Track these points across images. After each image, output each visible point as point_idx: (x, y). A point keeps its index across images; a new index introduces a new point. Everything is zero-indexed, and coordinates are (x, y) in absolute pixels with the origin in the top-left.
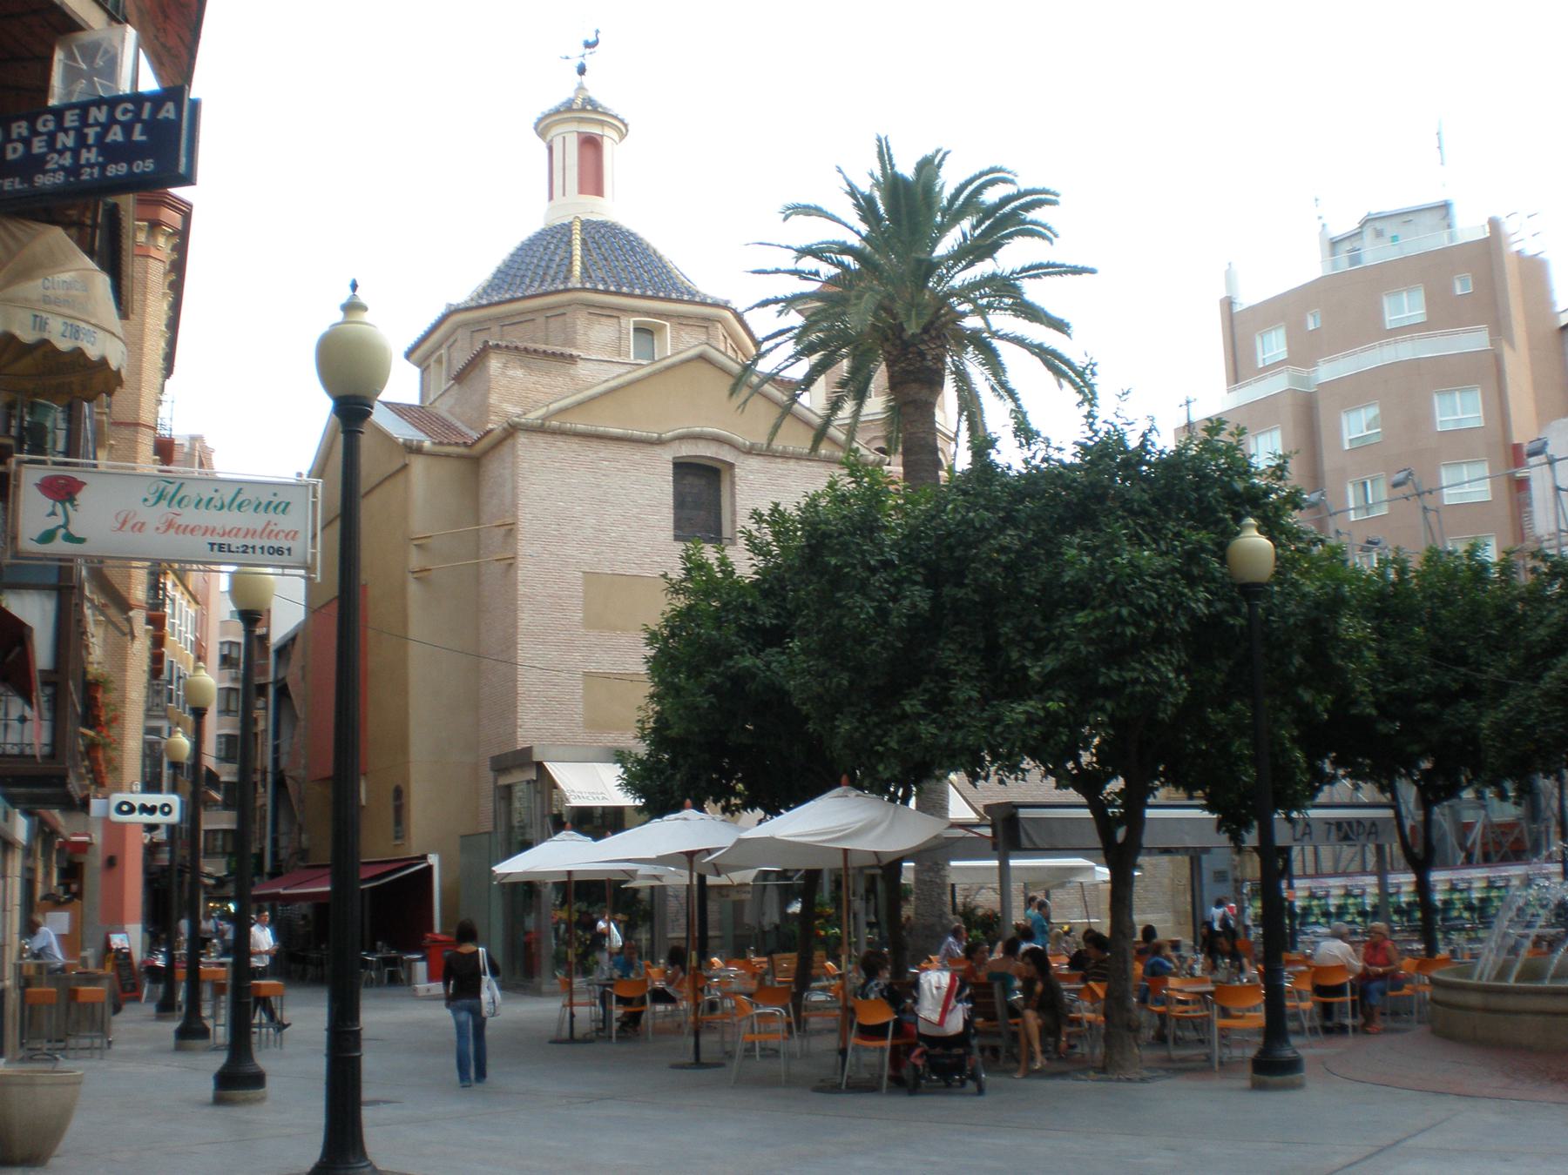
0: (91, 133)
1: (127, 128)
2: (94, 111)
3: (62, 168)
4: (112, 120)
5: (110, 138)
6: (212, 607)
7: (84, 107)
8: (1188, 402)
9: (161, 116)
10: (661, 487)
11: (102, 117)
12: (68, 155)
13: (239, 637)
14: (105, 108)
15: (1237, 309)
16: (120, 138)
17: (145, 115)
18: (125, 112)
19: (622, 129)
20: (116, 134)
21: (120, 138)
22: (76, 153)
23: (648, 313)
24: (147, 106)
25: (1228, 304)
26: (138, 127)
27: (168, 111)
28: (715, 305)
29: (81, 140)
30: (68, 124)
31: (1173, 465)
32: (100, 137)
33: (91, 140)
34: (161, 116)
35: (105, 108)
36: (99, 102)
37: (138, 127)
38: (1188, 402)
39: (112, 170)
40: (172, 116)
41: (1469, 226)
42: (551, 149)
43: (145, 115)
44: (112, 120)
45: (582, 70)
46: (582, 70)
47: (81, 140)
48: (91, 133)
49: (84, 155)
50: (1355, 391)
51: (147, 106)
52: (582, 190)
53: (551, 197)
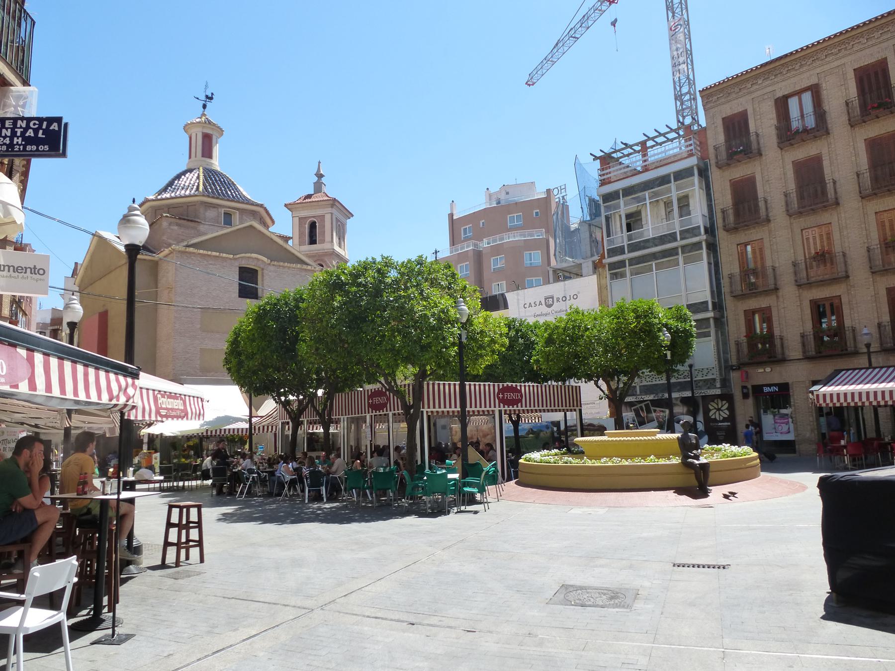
0: (19, 131)
1: (36, 131)
2: (19, 122)
3: (5, 144)
4: (28, 127)
5: (27, 134)
6: (33, 318)
7: (15, 120)
8: (436, 252)
9: (51, 128)
10: (233, 279)
11: (24, 125)
12: (8, 139)
13: (809, 326)
14: (25, 122)
15: (455, 218)
16: (32, 135)
17: (44, 127)
18: (34, 124)
19: (221, 131)
20: (30, 133)
21: (32, 135)
22: (12, 140)
23: (230, 208)
24: (45, 124)
25: (451, 216)
26: (41, 132)
27: (55, 126)
28: (258, 205)
29: (14, 134)
30: (7, 126)
31: (238, 384)
32: (23, 134)
33: (19, 134)
34: (51, 128)
35: (25, 122)
36: (22, 119)
37: (41, 132)
38: (436, 252)
39: (29, 148)
40: (56, 129)
41: (539, 193)
42: (190, 138)
43: (44, 127)
44: (28, 127)
45: (204, 106)
46: (204, 106)
47: (14, 134)
48: (19, 131)
49: (15, 140)
50: (497, 250)
51: (45, 124)
52: (203, 156)
53: (190, 157)
